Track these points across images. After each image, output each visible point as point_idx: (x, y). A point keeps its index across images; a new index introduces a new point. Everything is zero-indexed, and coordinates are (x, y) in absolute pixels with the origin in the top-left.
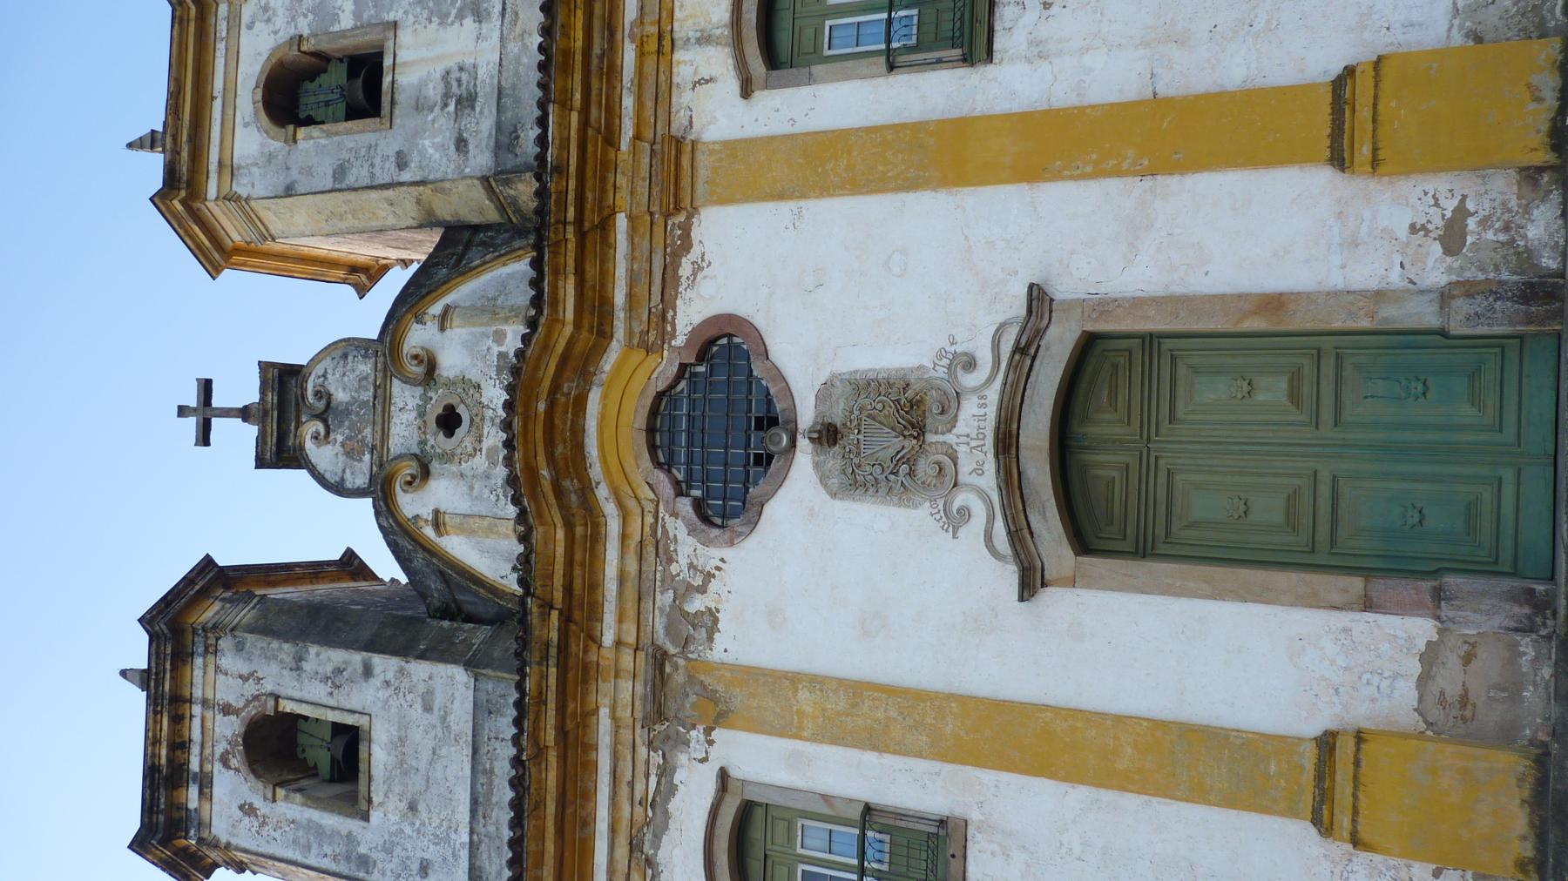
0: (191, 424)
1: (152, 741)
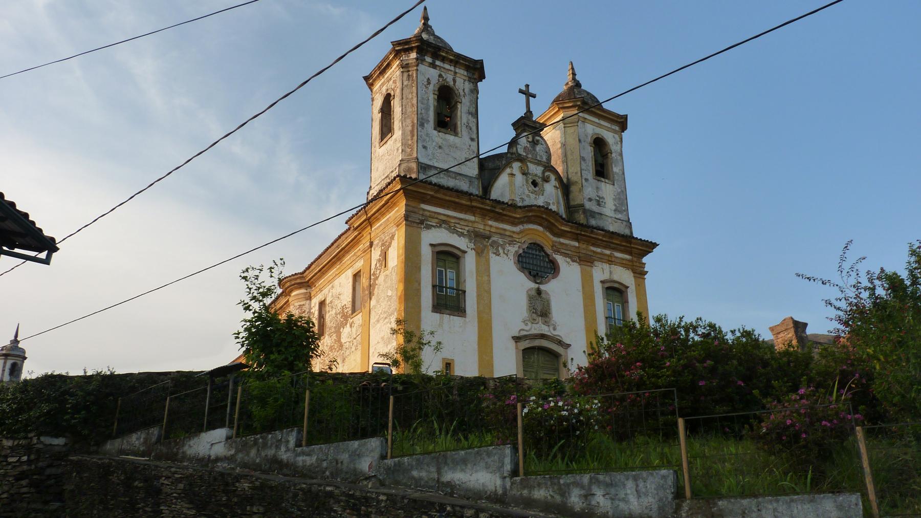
0: (524, 88)
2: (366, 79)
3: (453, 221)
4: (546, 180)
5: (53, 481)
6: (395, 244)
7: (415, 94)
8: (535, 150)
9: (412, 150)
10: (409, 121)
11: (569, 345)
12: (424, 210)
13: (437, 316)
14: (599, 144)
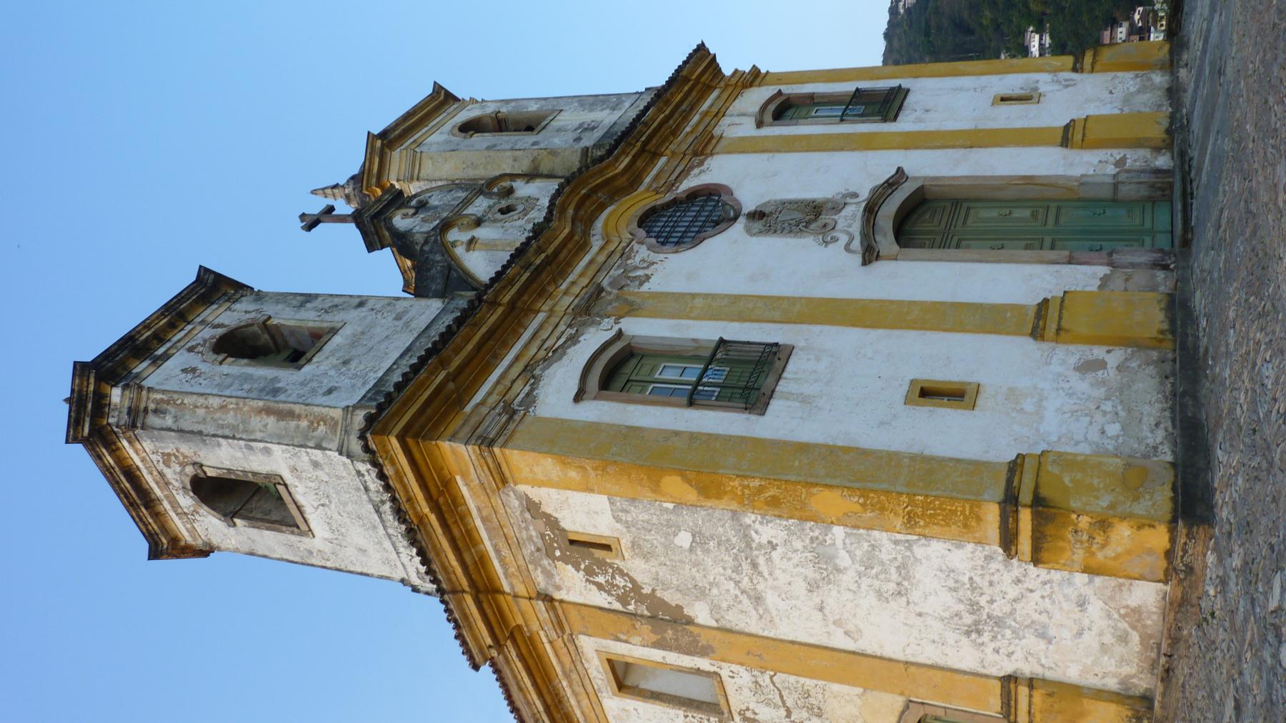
1: (146, 325)
2: (155, 554)
3: (533, 350)
4: (510, 191)
6: (550, 499)
7: (201, 401)
8: (436, 207)
9: (323, 419)
10: (256, 422)
11: (900, 170)
12: (482, 403)
13: (775, 405)
14: (468, 128)
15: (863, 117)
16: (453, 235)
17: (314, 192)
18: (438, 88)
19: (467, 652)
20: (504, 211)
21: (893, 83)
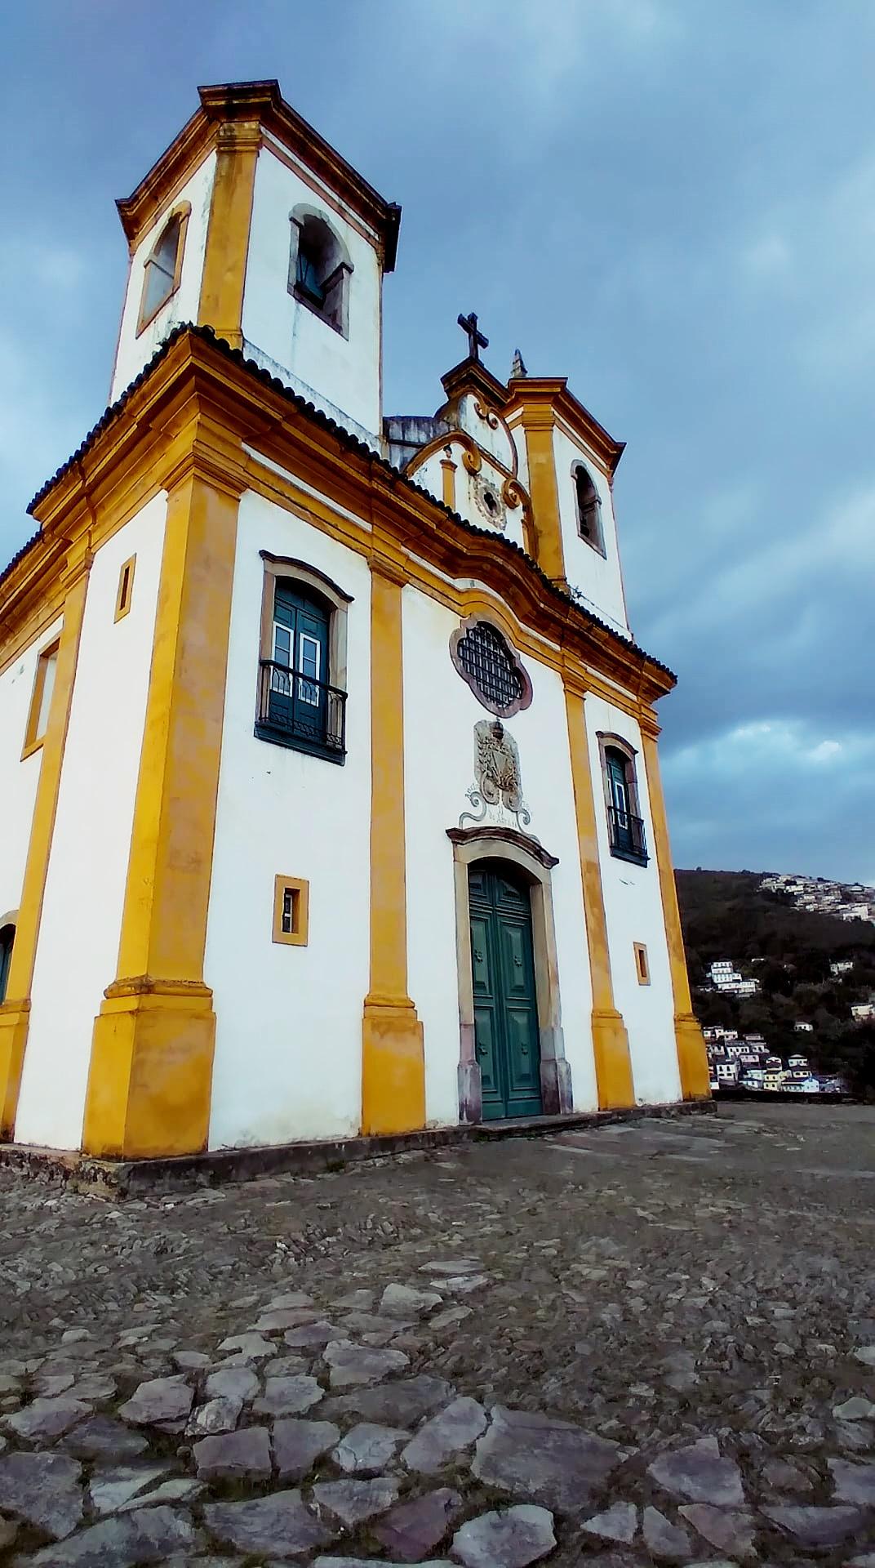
2: (122, 205)
5: (460, 1313)
11: (555, 861)
15: (616, 830)
16: (458, 450)
17: (517, 352)
18: (620, 448)
19: (40, 497)
20: (489, 499)
21: (651, 852)
